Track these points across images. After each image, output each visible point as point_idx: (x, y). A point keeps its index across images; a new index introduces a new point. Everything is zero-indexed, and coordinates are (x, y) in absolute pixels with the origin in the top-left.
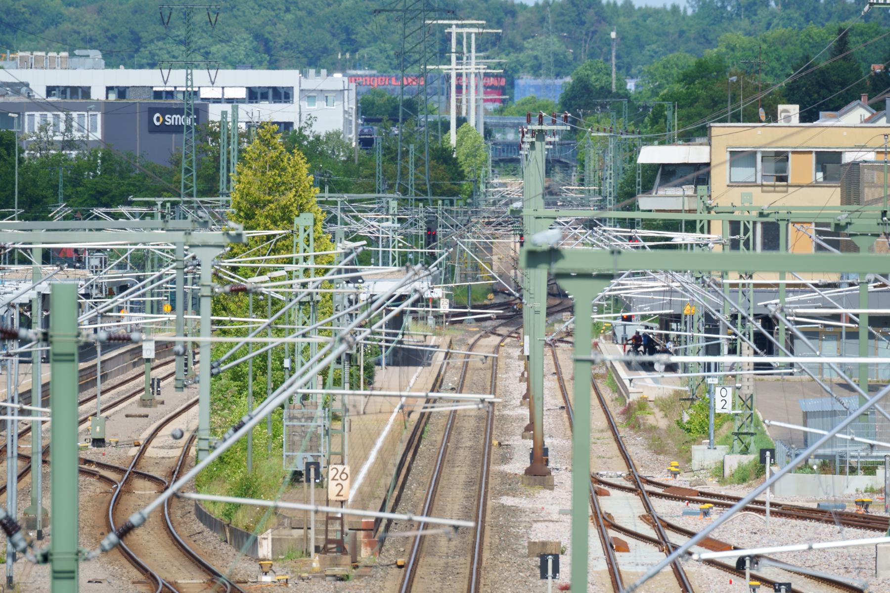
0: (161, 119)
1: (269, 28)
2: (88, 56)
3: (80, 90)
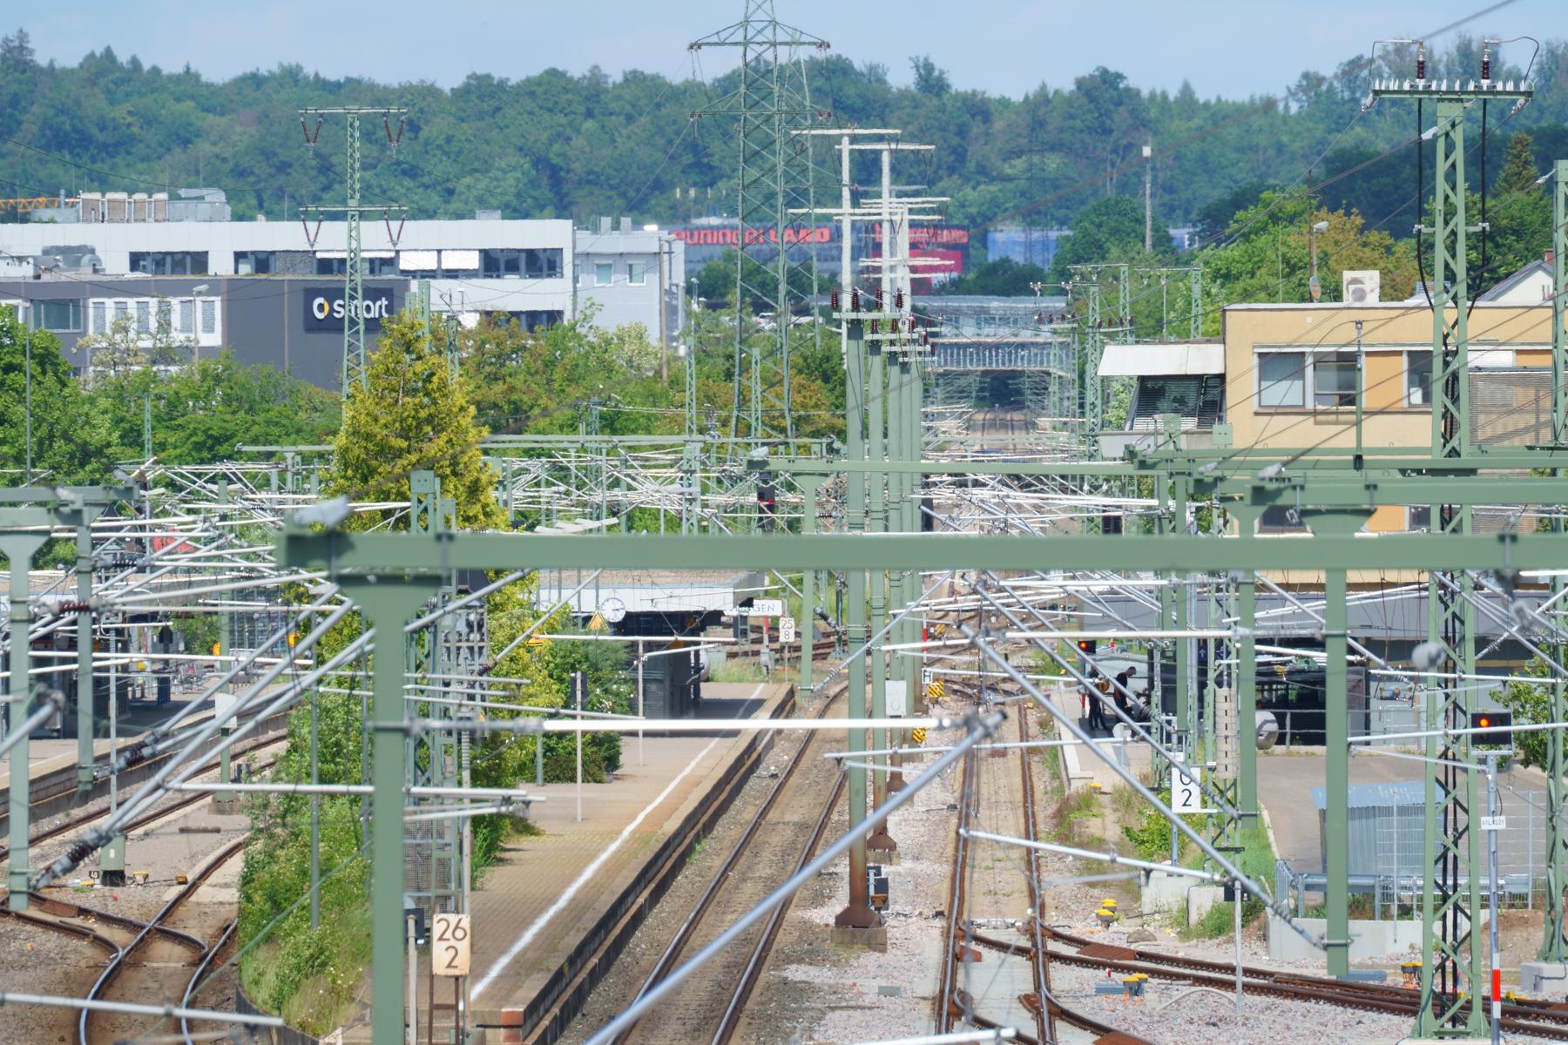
0: (327, 308)
1: (556, 147)
2: (202, 198)
3: (188, 259)
